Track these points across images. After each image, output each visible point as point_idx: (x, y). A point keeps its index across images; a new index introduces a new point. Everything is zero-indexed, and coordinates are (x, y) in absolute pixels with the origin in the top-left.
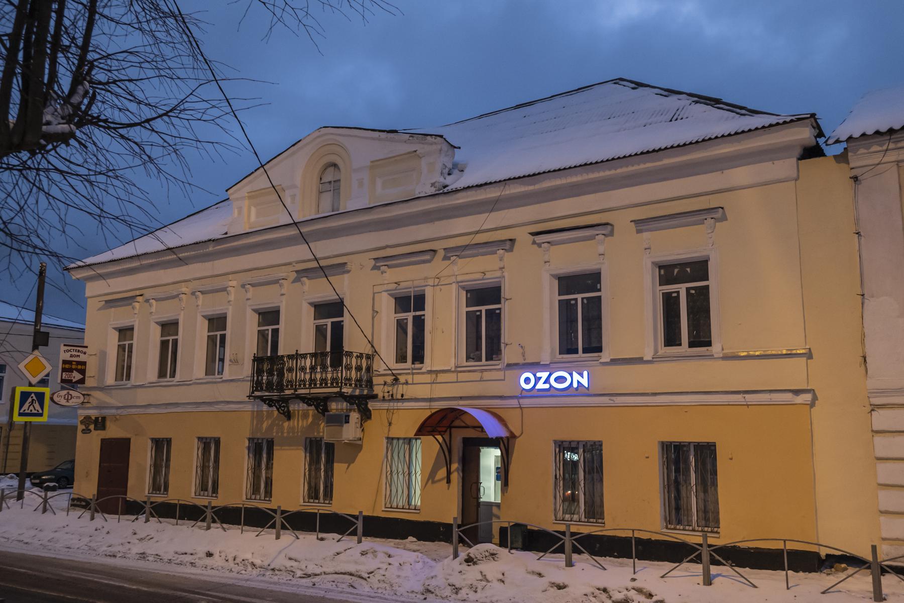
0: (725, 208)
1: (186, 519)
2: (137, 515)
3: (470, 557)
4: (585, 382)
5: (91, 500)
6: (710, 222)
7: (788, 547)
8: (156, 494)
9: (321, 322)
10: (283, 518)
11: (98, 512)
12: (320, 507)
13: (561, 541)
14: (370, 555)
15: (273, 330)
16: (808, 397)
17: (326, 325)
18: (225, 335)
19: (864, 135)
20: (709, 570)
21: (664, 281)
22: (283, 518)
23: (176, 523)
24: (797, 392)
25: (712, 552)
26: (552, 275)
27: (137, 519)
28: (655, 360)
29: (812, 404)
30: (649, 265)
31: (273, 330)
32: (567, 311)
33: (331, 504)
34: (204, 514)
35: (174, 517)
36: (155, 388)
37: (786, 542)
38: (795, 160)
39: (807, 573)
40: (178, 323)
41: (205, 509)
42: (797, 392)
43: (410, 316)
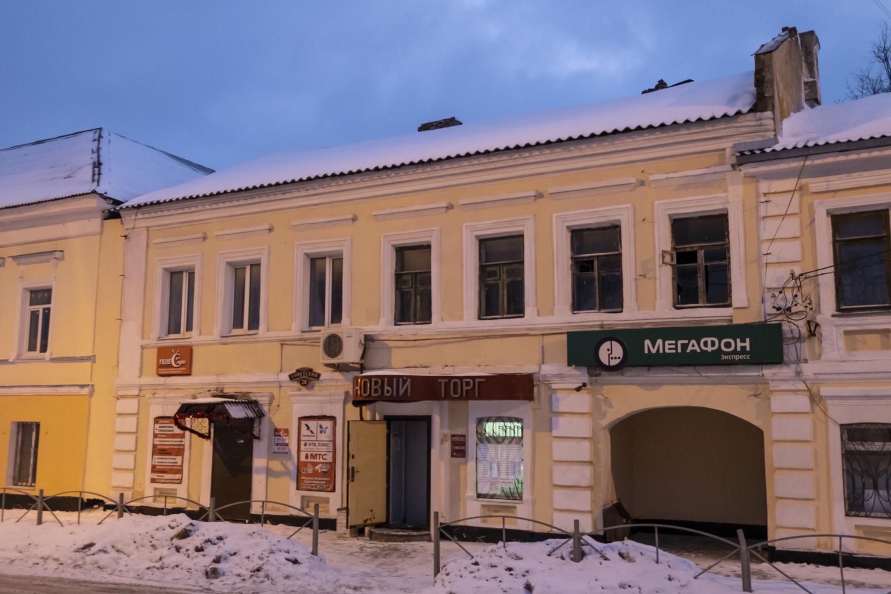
0: (65, 251)
1: (247, 521)
2: (27, 509)
3: (272, 550)
4: (647, 342)
5: (37, 497)
6: (53, 261)
7: (508, 527)
8: (22, 485)
9: (35, 308)
10: (218, 512)
11: (45, 509)
12: (22, 490)
13: (736, 543)
14: (232, 553)
15: (44, 309)
16: (86, 390)
17: (39, 311)
18: (49, 309)
19: (687, 122)
20: (748, 567)
21: (32, 303)
22: (218, 512)
23: (76, 520)
24: (82, 386)
25: (442, 530)
26: (25, 289)
27: (325, 532)
28: (15, 361)
29: (91, 394)
30: (20, 290)
31: (44, 309)
32: (581, 267)
33: (34, 486)
34: (205, 513)
35: (260, 522)
36: (689, 316)
37: (506, 519)
38: (99, 220)
39: (805, 564)
40: (342, 259)
41: (36, 499)
42: (82, 386)
43: (40, 308)
